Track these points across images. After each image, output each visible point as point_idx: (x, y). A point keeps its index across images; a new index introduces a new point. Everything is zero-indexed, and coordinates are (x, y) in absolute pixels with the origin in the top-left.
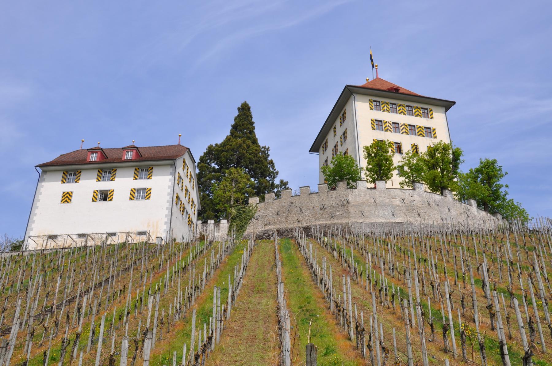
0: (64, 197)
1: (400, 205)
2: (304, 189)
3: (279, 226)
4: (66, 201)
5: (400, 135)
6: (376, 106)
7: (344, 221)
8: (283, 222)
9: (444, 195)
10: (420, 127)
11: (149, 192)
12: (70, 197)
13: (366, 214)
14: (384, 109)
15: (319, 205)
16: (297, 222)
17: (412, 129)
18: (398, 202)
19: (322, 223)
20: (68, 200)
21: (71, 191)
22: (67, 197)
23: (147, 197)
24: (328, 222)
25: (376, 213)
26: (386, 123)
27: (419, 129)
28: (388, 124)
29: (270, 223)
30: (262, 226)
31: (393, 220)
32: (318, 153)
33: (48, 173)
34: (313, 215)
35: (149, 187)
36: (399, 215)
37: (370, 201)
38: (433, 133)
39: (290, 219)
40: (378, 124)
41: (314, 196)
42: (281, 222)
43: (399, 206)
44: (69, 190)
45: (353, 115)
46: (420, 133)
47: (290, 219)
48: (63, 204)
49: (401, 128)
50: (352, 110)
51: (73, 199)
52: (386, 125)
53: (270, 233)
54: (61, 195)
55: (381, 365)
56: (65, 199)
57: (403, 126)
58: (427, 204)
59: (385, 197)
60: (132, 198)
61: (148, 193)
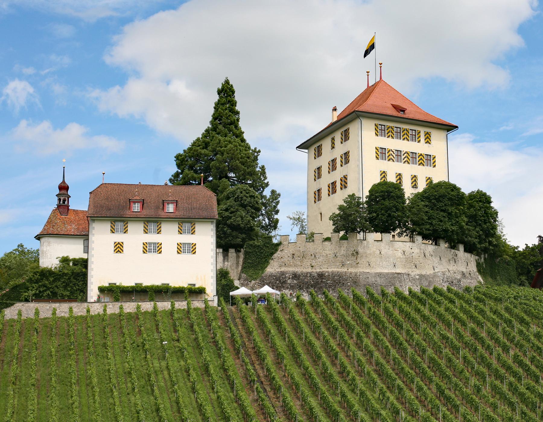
0: (116, 247)
1: (401, 257)
2: (318, 236)
3: (291, 269)
5: (401, 164)
6: (380, 131)
7: (352, 270)
8: (299, 265)
9: (438, 244)
10: (421, 155)
11: (194, 248)
12: (121, 247)
13: (372, 265)
15: (331, 253)
16: (310, 268)
18: (399, 254)
19: (334, 270)
20: (120, 250)
21: (122, 241)
23: (193, 252)
26: (389, 151)
28: (391, 152)
29: (285, 265)
31: (394, 271)
32: (307, 151)
33: (95, 221)
34: (326, 262)
36: (399, 266)
37: (376, 253)
38: (432, 162)
39: (304, 264)
41: (327, 244)
43: (400, 258)
44: (120, 241)
45: (358, 142)
46: (420, 161)
47: (304, 264)
50: (358, 136)
51: (125, 249)
52: (389, 154)
53: (287, 275)
54: (113, 245)
56: (118, 249)
57: (406, 155)
58: (423, 255)
60: (180, 252)
61: (193, 248)
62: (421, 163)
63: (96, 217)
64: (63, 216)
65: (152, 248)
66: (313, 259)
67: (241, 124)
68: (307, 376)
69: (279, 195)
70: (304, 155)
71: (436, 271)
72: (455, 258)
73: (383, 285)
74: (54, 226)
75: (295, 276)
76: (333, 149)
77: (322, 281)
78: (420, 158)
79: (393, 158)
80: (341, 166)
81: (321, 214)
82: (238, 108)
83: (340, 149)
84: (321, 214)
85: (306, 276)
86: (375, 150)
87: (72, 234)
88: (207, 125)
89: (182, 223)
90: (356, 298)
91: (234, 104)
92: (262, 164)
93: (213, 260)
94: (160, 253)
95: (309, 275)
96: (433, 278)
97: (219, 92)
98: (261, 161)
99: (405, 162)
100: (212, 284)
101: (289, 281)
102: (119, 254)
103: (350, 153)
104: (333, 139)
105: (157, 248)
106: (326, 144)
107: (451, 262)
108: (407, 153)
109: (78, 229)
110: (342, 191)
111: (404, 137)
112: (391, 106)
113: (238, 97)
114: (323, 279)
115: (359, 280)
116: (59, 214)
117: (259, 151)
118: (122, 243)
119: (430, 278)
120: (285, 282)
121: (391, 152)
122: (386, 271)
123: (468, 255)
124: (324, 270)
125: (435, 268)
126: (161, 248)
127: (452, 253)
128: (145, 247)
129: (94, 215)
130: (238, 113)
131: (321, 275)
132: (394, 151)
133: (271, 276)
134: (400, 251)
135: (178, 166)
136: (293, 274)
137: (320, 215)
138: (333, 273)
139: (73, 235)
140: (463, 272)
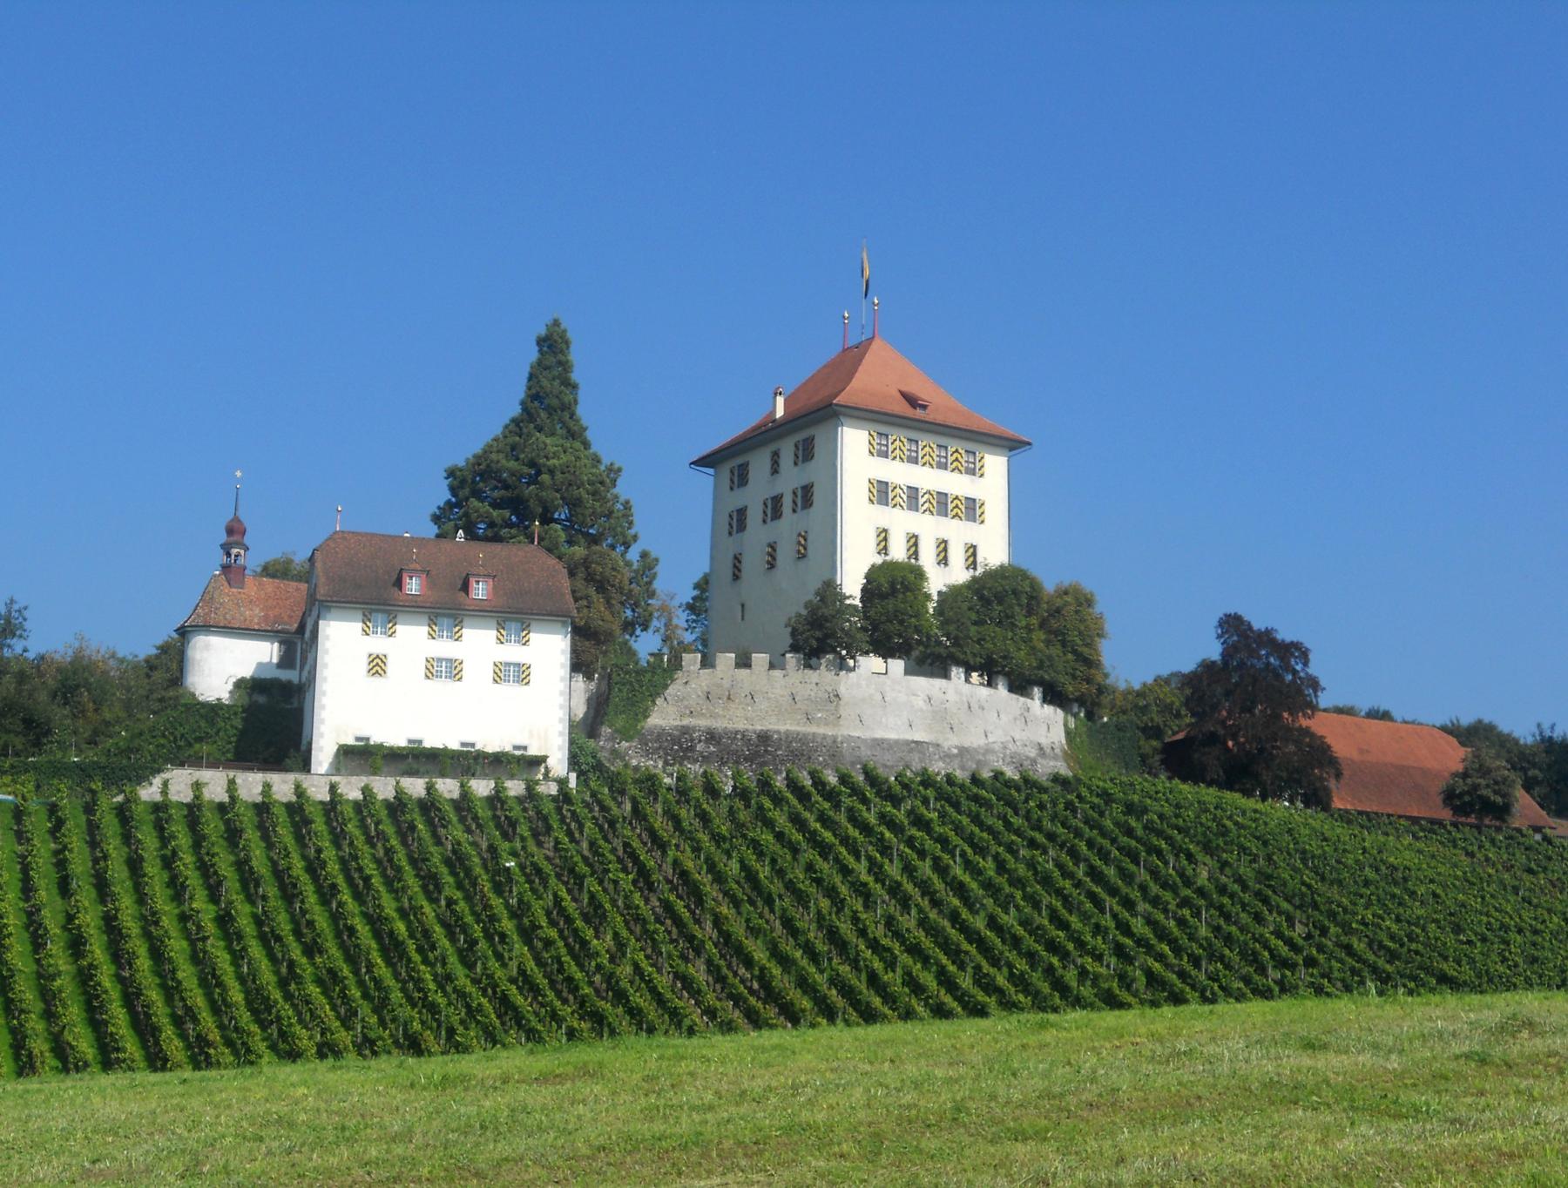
0: (372, 665)
3: (703, 723)
4: (377, 672)
7: (830, 732)
10: (957, 498)
12: (382, 665)
14: (894, 455)
17: (942, 504)
18: (920, 703)
20: (380, 671)
21: (384, 653)
22: (377, 664)
23: (525, 681)
24: (799, 729)
25: (884, 720)
26: (895, 488)
27: (956, 502)
28: (898, 490)
30: (674, 717)
32: (711, 471)
33: (332, 610)
35: (460, 657)
38: (978, 512)
40: (882, 492)
42: (713, 716)
43: (921, 710)
48: (373, 679)
49: (921, 501)
51: (389, 669)
52: (894, 494)
54: (365, 661)
55: (1, 628)
57: (926, 496)
59: (900, 692)
60: (498, 679)
62: (957, 515)
63: (336, 602)
64: (234, 590)
65: (443, 669)
66: (748, 705)
67: (581, 411)
68: (149, 921)
69: (657, 560)
70: (705, 480)
71: (991, 740)
72: (1026, 714)
73: (888, 763)
74: (216, 609)
75: (712, 736)
76: (776, 475)
77: (766, 751)
78: (954, 505)
79: (902, 503)
80: (794, 511)
81: (743, 606)
82: (575, 376)
83: (791, 478)
84: (743, 606)
85: (735, 738)
86: (867, 485)
87: (256, 627)
88: (516, 410)
89: (504, 622)
90: (793, 785)
91: (566, 366)
92: (627, 498)
93: (562, 700)
94: (460, 679)
95: (739, 736)
96: (984, 755)
97: (541, 342)
98: (623, 489)
99: (925, 511)
100: (560, 748)
101: (699, 747)
102: (377, 679)
103: (815, 488)
104: (776, 456)
105: (452, 670)
106: (759, 463)
107: (1018, 722)
108: (929, 492)
109: (266, 617)
110: (731, 538)
111: (924, 460)
112: (899, 394)
113: (575, 355)
114: (769, 746)
115: (841, 752)
116: (226, 583)
117: (619, 470)
118: (370, 655)
119: (978, 753)
120: (692, 749)
121: (898, 490)
122: (892, 736)
123: (1049, 710)
124: (770, 727)
125: (989, 735)
126: (461, 670)
127: (1020, 704)
128: (431, 668)
129: (331, 597)
130: (575, 387)
131: (764, 737)
132: (934, 494)
133: (661, 735)
134: (923, 696)
135: (453, 490)
136: (707, 733)
137: (740, 607)
138: (787, 733)
139: (258, 630)
140: (1039, 744)
